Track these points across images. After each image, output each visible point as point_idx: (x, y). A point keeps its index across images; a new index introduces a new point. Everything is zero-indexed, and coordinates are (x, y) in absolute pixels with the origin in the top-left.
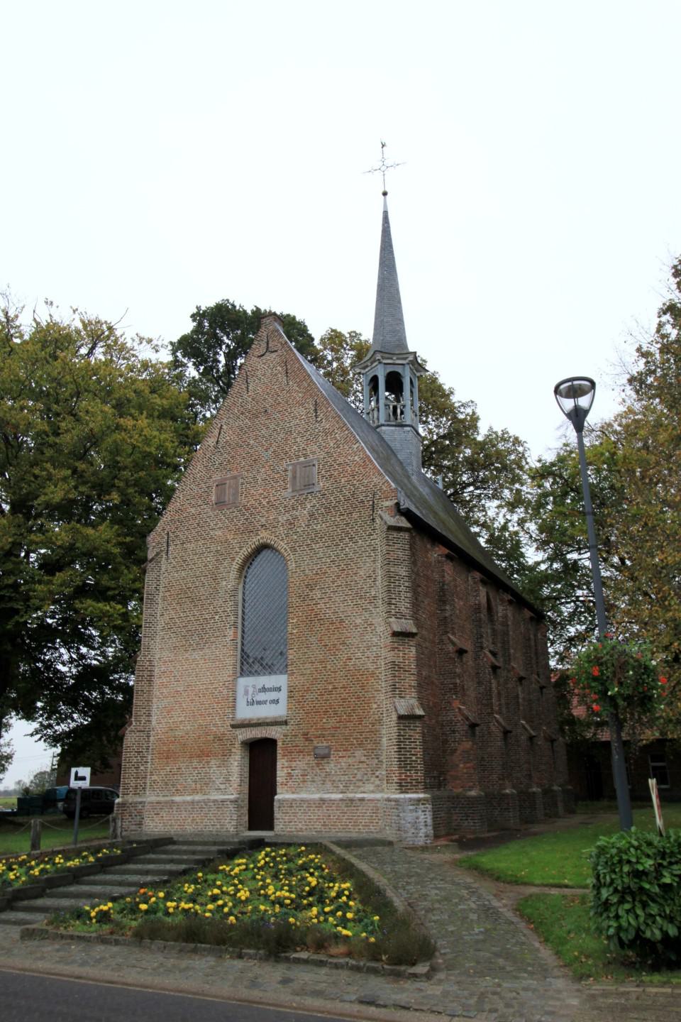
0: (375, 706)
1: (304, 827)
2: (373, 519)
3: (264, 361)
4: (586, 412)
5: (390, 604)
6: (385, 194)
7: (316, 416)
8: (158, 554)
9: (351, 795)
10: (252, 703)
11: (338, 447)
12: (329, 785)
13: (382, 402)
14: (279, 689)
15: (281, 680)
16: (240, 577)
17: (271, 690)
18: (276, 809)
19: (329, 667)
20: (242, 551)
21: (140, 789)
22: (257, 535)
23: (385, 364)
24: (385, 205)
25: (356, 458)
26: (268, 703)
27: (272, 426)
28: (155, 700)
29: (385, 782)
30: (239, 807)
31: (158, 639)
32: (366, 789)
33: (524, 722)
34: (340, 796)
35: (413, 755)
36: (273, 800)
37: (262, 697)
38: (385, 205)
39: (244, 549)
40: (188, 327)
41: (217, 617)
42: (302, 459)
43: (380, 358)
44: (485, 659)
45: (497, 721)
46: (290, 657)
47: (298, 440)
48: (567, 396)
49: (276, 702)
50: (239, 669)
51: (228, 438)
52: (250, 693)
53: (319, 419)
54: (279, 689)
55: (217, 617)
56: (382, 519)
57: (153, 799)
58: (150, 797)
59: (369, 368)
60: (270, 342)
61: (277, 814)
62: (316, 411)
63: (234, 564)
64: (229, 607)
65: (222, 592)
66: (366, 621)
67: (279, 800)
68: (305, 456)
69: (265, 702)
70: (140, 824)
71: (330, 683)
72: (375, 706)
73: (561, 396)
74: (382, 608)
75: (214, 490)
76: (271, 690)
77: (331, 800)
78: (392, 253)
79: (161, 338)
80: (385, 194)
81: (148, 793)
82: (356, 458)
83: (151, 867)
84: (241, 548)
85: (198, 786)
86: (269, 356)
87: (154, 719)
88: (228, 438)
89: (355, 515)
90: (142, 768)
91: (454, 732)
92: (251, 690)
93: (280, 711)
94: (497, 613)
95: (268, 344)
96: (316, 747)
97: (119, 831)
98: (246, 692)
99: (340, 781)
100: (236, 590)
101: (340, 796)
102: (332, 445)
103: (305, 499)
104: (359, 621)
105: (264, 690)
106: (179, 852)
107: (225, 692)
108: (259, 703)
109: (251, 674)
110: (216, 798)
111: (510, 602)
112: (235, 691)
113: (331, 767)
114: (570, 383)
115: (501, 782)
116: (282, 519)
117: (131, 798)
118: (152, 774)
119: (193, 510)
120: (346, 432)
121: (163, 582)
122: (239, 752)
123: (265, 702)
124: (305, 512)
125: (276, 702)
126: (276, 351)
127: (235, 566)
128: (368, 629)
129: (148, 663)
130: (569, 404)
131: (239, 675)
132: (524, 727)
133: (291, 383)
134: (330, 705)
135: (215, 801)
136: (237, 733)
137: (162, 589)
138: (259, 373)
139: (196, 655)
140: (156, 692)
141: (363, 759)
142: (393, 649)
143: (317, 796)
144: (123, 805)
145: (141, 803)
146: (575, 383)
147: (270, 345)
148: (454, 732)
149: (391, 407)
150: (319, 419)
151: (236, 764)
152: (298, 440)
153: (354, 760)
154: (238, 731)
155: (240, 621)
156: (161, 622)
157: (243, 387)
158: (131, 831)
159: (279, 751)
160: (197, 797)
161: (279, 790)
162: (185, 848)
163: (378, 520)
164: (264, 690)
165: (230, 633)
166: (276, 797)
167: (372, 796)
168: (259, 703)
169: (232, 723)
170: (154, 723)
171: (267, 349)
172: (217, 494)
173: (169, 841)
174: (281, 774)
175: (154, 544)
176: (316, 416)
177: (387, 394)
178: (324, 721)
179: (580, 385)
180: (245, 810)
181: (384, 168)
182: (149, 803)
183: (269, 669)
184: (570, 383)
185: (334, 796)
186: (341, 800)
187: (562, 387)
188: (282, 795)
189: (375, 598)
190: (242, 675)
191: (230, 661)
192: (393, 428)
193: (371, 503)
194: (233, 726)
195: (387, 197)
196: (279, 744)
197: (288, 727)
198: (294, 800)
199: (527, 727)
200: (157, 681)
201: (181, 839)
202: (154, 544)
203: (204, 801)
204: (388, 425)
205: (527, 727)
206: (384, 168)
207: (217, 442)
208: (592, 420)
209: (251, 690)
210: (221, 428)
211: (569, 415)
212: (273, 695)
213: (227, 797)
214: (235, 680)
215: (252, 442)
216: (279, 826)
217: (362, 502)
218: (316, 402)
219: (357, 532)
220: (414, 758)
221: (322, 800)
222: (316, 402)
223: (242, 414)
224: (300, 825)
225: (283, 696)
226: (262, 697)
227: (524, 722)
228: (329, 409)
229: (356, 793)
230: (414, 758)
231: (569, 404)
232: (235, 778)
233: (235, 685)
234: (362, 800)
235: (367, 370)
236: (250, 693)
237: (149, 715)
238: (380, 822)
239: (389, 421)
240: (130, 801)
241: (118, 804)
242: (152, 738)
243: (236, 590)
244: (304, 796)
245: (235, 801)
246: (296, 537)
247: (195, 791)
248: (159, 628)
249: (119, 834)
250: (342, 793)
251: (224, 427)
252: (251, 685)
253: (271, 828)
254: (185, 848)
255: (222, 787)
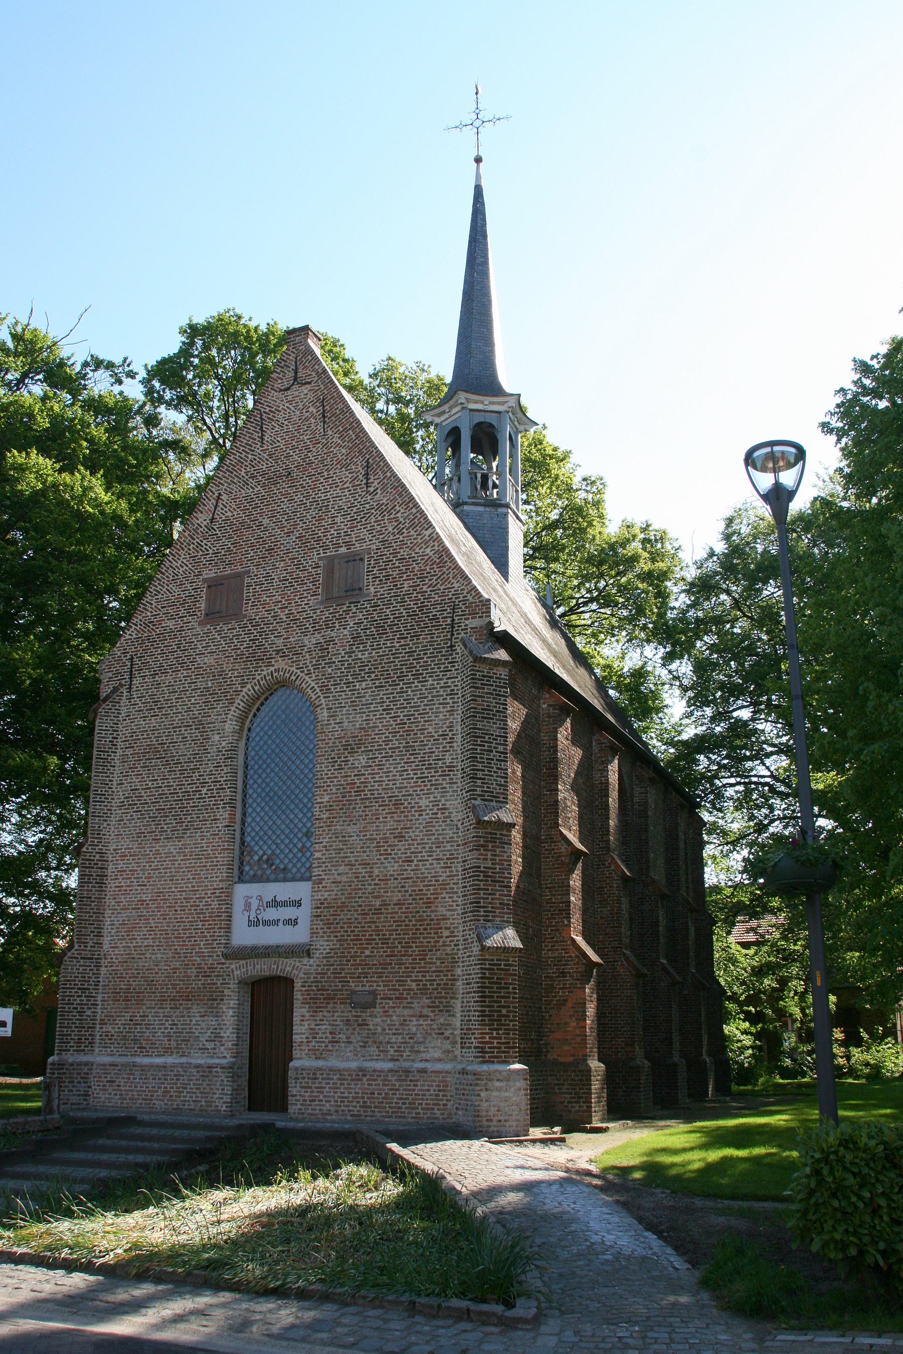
0: (446, 933)
1: (333, 1109)
2: (452, 646)
3: (290, 398)
4: (791, 494)
5: (474, 778)
6: (478, 160)
7: (367, 485)
8: (115, 690)
9: (407, 1064)
10: (254, 923)
11: (400, 532)
12: (373, 1050)
13: (465, 468)
14: (298, 904)
15: (301, 890)
16: (242, 729)
17: (284, 904)
18: (291, 1082)
19: (376, 872)
20: (245, 690)
21: (85, 1044)
22: (270, 665)
23: (471, 410)
24: (478, 177)
25: (428, 551)
26: (281, 923)
27: (299, 497)
28: (108, 912)
29: (459, 1045)
30: (235, 1077)
31: (113, 820)
32: (428, 1056)
33: (665, 962)
34: (389, 1065)
35: (504, 1007)
36: (286, 1069)
37: (271, 914)
38: (478, 177)
39: (249, 686)
40: (172, 345)
41: (204, 791)
42: (343, 550)
43: (463, 401)
44: (613, 867)
45: (627, 959)
46: (318, 855)
47: (338, 520)
48: (764, 469)
49: (295, 922)
50: (236, 871)
51: (229, 514)
52: (254, 907)
53: (372, 489)
54: (298, 904)
55: (204, 791)
56: (466, 647)
57: (106, 1059)
58: (101, 1058)
59: (446, 416)
60: (300, 367)
61: (294, 1089)
62: (367, 475)
63: (233, 708)
64: (223, 775)
65: (213, 751)
66: (436, 803)
67: (296, 1069)
68: (348, 544)
69: (276, 922)
70: (86, 1095)
71: (376, 897)
72: (446, 933)
73: (755, 468)
74: (460, 782)
75: (203, 595)
76: (284, 904)
77: (374, 1071)
78: (483, 204)
79: (128, 362)
80: (478, 160)
81: (97, 1050)
82: (428, 551)
83: (105, 1157)
84: (243, 685)
85: (173, 1043)
86: (296, 391)
87: (106, 941)
88: (229, 514)
89: (424, 639)
90: (89, 1013)
91: (563, 974)
92: (255, 904)
93: (299, 935)
94: (632, 796)
95: (296, 372)
96: (354, 992)
97: (56, 1103)
98: (248, 907)
99: (388, 1043)
100: (234, 749)
101: (389, 1065)
102: (390, 529)
103: (347, 612)
104: (424, 803)
105: (275, 903)
106: (142, 1138)
107: (215, 904)
108: (267, 923)
109: (255, 879)
110: (200, 1061)
111: (652, 781)
112: (230, 906)
113: (376, 1021)
114: (768, 449)
115: (629, 1049)
116: (310, 641)
117: (70, 1058)
118: (103, 1023)
119: (171, 624)
120: (414, 510)
121: (123, 731)
122: (235, 996)
123: (276, 922)
124: (346, 632)
125: (295, 922)
126: (309, 383)
127: (233, 712)
128: (439, 816)
129: (98, 856)
130: (766, 481)
131: (236, 879)
132: (664, 969)
133: (330, 432)
134: (377, 931)
135: (197, 1066)
136: (233, 966)
137: (120, 744)
138: (280, 416)
139: (172, 847)
140: (109, 901)
141: (426, 1011)
142: (477, 848)
143: (354, 1065)
144: (61, 1065)
145: (86, 1064)
146: (776, 448)
147: (299, 375)
148: (563, 974)
149: (479, 476)
150: (372, 489)
151: (231, 1012)
152: (338, 520)
153: (410, 1012)
154: (233, 965)
155: (239, 797)
156: (119, 794)
157: (256, 436)
158: (72, 1104)
159: (298, 995)
160: (170, 1060)
161: (296, 1053)
162: (155, 1131)
163: (459, 648)
164: (275, 903)
165: (223, 815)
166: (291, 1064)
167: (439, 1066)
168: (267, 923)
169: (225, 951)
170: (106, 946)
171: (295, 379)
172: (208, 600)
173: (130, 1120)
174: (300, 1030)
175: (110, 675)
176: (367, 485)
177: (472, 455)
178: (367, 952)
179: (783, 452)
180: (244, 1082)
181: (478, 123)
182: (99, 1065)
183: (284, 875)
184: (768, 449)
185: (379, 1065)
186: (390, 1071)
187: (756, 454)
188: (301, 1061)
189: (451, 768)
190: (241, 880)
191: (223, 858)
192: (481, 509)
193: (449, 620)
194: (226, 956)
195: (481, 165)
196: (298, 985)
197: (312, 961)
198: (320, 1069)
199: (669, 967)
200: (111, 885)
201: (146, 1117)
202: (110, 675)
203: (181, 1065)
204: (473, 504)
205: (669, 967)
206: (478, 123)
207: (212, 520)
208: (799, 504)
209: (255, 904)
210: (219, 498)
211: (766, 497)
212: (289, 913)
213: (217, 1061)
214: (231, 886)
215: (265, 521)
216: (293, 1109)
217: (435, 618)
218: (367, 461)
219: (426, 666)
220: (504, 1011)
221: (361, 1069)
222: (367, 461)
223: (253, 477)
224: (327, 1104)
225: (304, 914)
226: (271, 914)
227: (665, 962)
228: (388, 474)
229: (413, 1060)
230: (504, 1011)
231: (766, 481)
232: (228, 1033)
233: (230, 895)
234: (424, 1071)
235: (443, 418)
236: (254, 907)
237: (99, 935)
238: (450, 1104)
239: (475, 497)
240: (71, 1060)
241: (53, 1064)
242: (103, 970)
243: (234, 749)
244: (334, 1063)
245: (231, 1067)
246: (330, 670)
247: (168, 1051)
248: (115, 803)
249: (55, 1108)
250: (392, 1060)
251: (224, 497)
252: (255, 896)
253: (283, 1107)
254: (155, 1131)
255: (210, 1045)
